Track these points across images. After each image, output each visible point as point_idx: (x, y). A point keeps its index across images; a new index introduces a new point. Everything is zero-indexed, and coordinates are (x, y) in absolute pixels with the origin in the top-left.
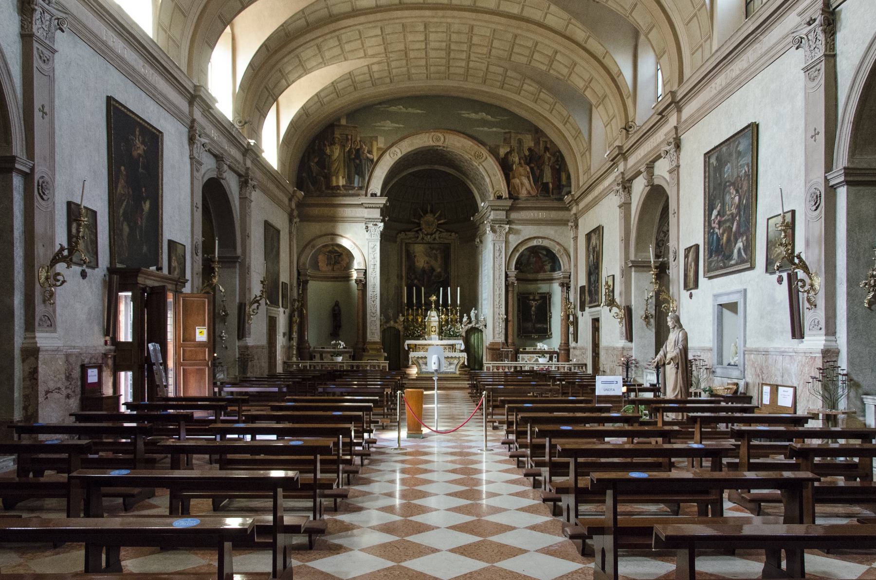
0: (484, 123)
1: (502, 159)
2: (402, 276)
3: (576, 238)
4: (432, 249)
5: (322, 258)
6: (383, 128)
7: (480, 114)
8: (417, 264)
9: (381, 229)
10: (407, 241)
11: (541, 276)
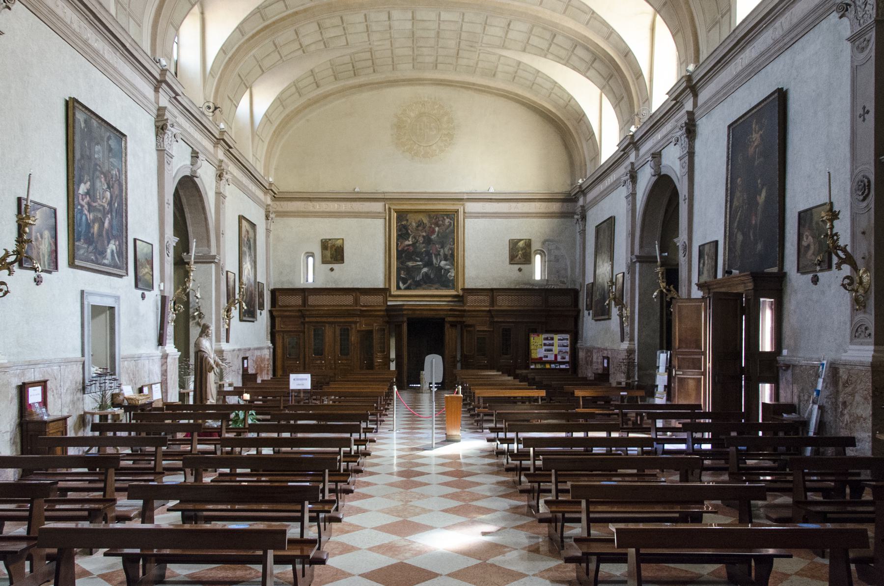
3: (583, 232)
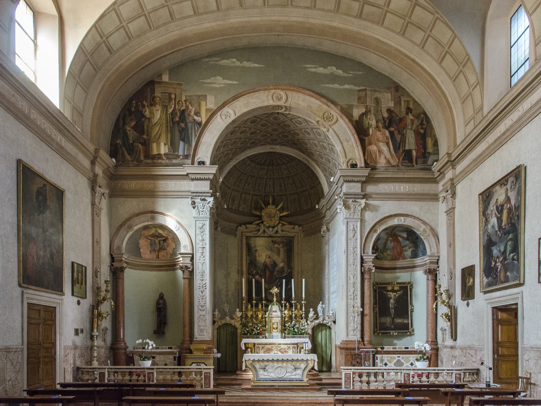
0: (334, 79)
1: (356, 122)
2: (242, 270)
4: (274, 242)
5: (143, 243)
6: (213, 85)
7: (329, 68)
8: (258, 258)
9: (211, 205)
10: (248, 234)
11: (400, 263)
